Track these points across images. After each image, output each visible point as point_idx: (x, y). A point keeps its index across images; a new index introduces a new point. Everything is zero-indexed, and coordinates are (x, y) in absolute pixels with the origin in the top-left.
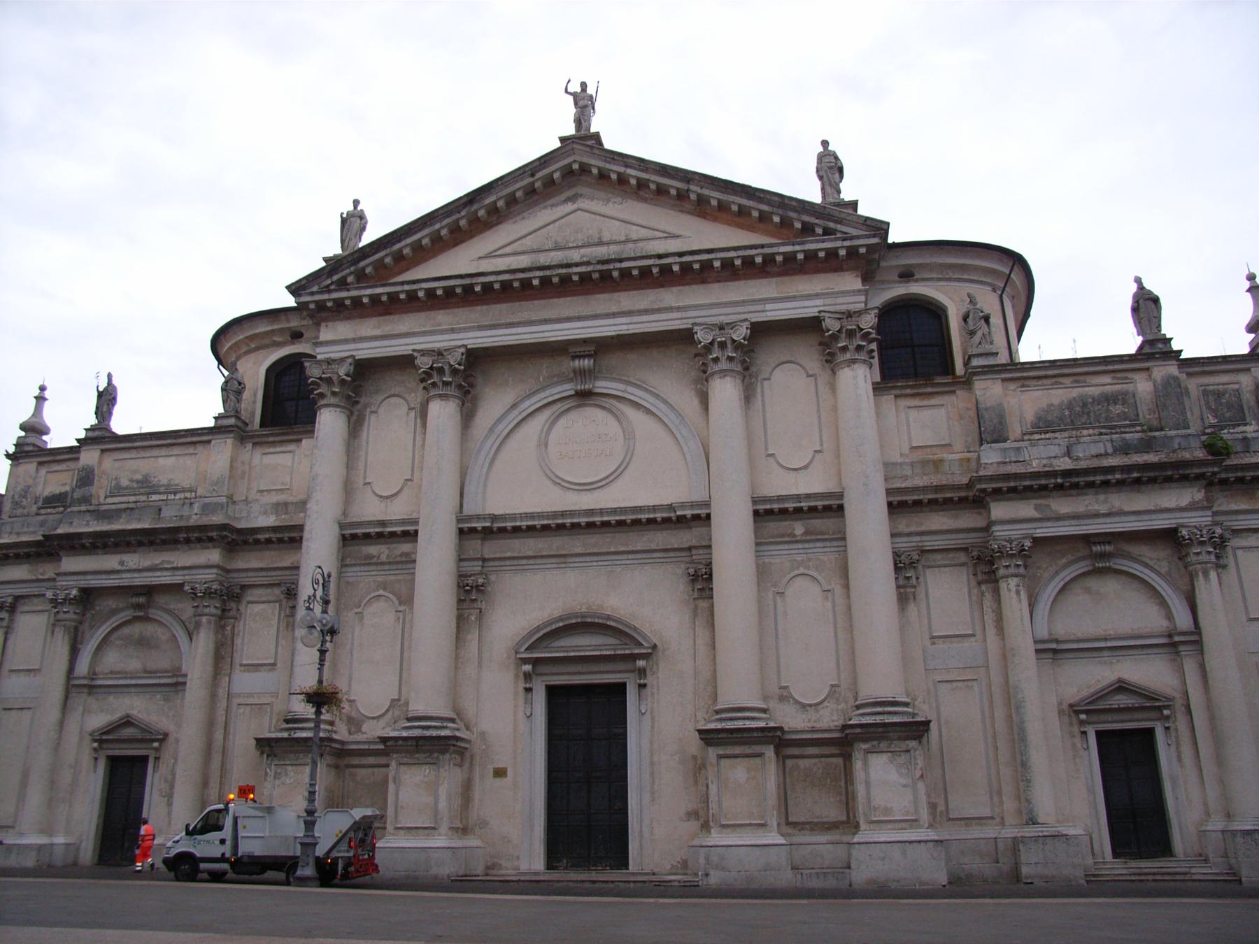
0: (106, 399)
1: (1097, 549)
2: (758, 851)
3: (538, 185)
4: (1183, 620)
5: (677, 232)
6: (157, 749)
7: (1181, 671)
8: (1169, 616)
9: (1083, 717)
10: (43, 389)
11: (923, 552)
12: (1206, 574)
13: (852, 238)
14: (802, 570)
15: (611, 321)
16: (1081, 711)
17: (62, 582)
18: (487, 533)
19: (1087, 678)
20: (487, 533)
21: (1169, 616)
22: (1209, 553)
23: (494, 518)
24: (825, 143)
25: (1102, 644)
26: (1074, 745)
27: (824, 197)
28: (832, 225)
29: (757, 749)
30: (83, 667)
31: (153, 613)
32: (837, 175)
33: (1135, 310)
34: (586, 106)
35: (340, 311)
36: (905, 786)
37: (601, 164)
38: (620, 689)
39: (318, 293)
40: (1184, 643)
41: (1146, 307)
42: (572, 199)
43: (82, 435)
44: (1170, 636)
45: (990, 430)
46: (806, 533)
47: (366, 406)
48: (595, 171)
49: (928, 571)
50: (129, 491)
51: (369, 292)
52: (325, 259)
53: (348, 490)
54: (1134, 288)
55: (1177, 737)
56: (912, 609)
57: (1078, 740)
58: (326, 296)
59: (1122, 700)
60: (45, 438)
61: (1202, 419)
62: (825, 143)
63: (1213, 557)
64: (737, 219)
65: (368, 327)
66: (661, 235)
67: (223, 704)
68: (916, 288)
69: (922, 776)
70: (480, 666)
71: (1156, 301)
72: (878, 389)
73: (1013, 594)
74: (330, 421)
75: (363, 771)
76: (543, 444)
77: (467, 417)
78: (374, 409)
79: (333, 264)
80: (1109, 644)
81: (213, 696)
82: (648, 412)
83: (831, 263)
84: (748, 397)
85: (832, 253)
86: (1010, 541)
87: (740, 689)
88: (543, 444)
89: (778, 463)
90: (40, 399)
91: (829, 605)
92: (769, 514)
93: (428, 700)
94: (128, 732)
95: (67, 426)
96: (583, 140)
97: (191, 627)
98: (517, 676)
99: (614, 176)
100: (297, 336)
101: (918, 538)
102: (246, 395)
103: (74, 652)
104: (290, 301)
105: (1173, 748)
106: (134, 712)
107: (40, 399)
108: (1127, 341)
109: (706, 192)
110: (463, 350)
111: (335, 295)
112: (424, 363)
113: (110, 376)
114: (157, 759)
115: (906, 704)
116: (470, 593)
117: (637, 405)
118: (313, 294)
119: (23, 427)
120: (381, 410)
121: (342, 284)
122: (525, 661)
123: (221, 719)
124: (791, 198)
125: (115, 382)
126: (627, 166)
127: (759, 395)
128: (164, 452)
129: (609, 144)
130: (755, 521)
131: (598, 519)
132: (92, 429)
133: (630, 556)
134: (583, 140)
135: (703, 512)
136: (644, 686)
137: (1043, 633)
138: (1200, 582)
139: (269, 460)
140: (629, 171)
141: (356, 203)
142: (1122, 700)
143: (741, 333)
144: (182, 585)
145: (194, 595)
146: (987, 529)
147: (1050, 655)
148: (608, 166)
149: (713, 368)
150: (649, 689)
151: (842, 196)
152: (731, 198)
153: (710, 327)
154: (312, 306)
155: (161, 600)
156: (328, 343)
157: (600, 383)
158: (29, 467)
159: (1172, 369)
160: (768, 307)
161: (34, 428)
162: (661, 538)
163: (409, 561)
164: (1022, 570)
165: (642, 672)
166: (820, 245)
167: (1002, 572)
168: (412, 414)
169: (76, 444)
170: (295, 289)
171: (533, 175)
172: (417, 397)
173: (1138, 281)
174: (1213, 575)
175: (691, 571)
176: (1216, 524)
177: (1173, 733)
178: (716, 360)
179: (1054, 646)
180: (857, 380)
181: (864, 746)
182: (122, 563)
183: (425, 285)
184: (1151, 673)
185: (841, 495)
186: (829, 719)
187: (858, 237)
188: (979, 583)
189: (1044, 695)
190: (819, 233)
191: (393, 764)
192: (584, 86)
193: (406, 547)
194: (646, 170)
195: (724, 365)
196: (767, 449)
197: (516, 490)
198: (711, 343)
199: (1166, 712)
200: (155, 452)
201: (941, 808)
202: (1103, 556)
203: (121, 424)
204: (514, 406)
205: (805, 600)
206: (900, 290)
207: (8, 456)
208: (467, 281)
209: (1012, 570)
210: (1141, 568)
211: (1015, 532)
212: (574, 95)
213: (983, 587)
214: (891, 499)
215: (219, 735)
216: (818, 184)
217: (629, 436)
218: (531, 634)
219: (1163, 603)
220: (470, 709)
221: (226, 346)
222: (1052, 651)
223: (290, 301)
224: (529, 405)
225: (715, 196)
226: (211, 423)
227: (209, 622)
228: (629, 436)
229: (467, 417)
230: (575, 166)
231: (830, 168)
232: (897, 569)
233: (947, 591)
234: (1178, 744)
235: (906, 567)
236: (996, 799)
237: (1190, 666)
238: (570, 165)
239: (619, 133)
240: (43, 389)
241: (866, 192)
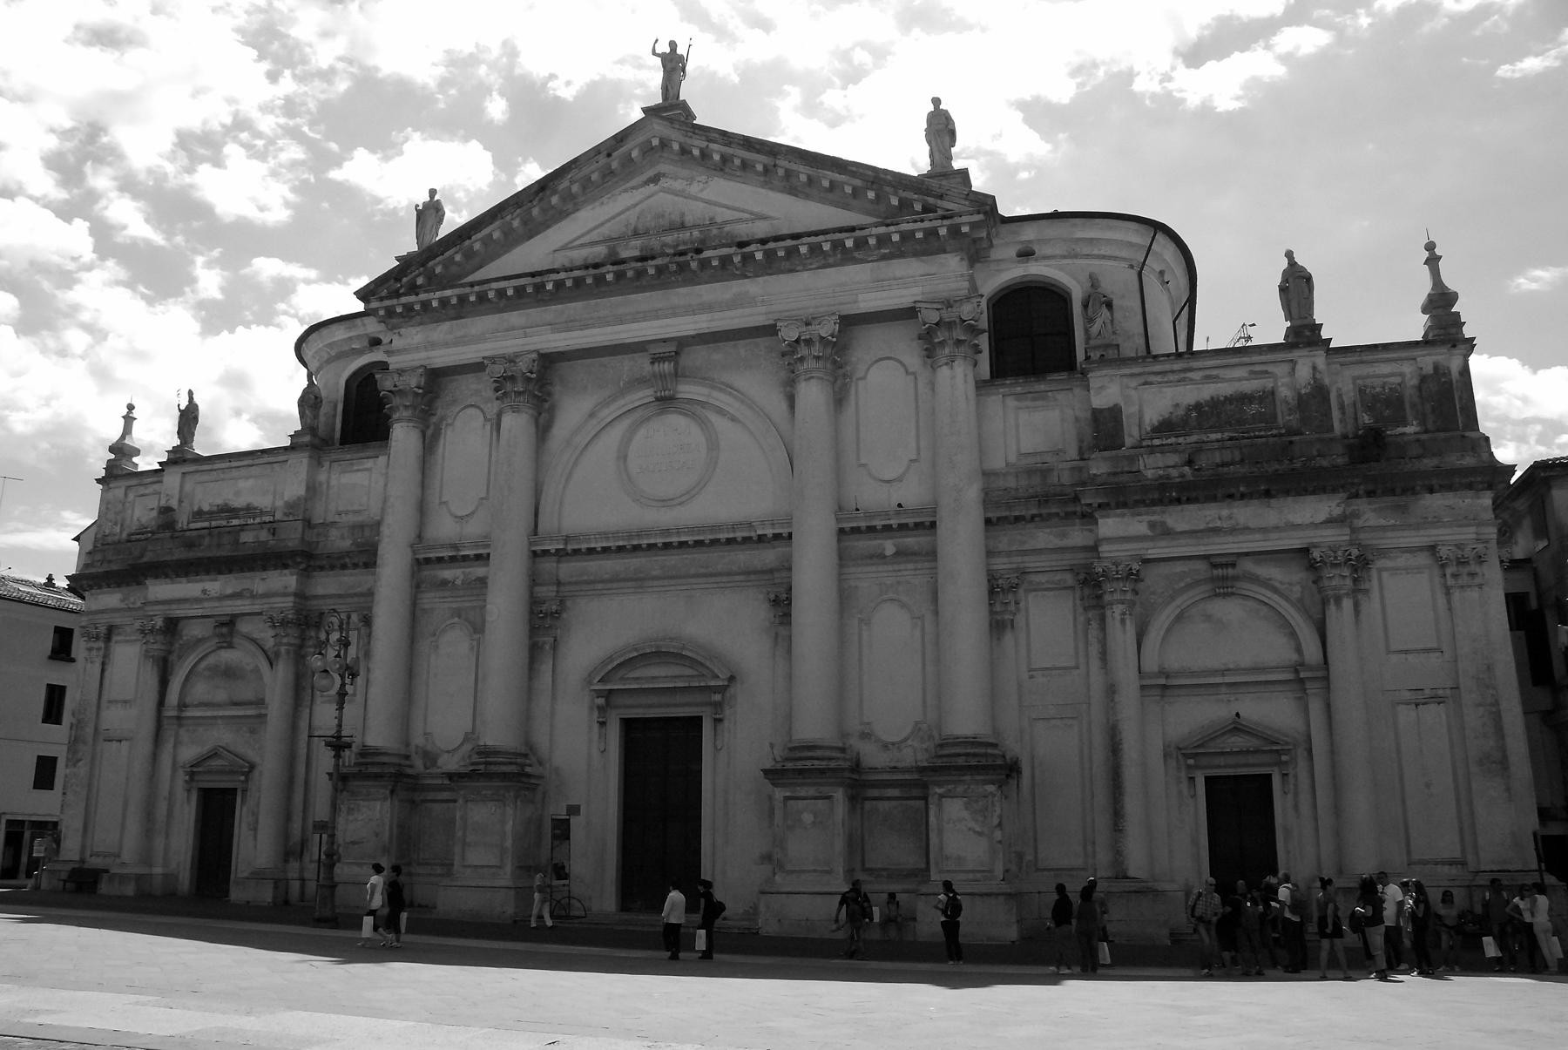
0: (188, 418)
2: (819, 899)
3: (615, 165)
4: (1312, 652)
7: (1306, 710)
9: (1191, 762)
10: (1430, 247)
11: (1146, 561)
12: (1338, 600)
14: (891, 595)
16: (1187, 754)
17: (151, 610)
18: (560, 554)
19: (1192, 716)
20: (560, 554)
22: (1344, 577)
23: (567, 539)
25: (1218, 680)
26: (1180, 792)
28: (931, 200)
29: (826, 790)
30: (173, 697)
32: (947, 139)
33: (1283, 290)
34: (674, 69)
36: (980, 834)
37: (682, 139)
38: (696, 722)
39: (386, 298)
40: (1310, 679)
42: (655, 179)
45: (1105, 429)
46: (897, 554)
47: (442, 419)
48: (676, 147)
49: (1031, 596)
50: (211, 515)
51: (438, 294)
52: (398, 259)
53: (422, 508)
54: (1285, 263)
55: (1296, 786)
56: (1008, 638)
57: (1184, 786)
58: (395, 301)
59: (1238, 742)
60: (135, 460)
61: (1356, 419)
63: (1349, 582)
64: (830, 196)
65: (442, 331)
67: (304, 736)
68: (1035, 269)
69: (1000, 825)
70: (554, 697)
71: (1308, 279)
72: (981, 386)
73: (1118, 624)
74: (403, 436)
75: (436, 806)
77: (543, 430)
78: (861, 374)
79: (406, 263)
80: (1228, 680)
81: (294, 728)
82: (733, 419)
83: (929, 246)
84: (839, 401)
85: (931, 233)
86: (1116, 564)
87: (813, 726)
89: (870, 474)
90: (1433, 261)
91: (918, 633)
92: (853, 532)
93: (499, 735)
94: (216, 763)
95: (155, 440)
96: (670, 110)
97: (272, 656)
98: (591, 708)
99: (696, 152)
100: (375, 342)
101: (1019, 559)
102: (325, 409)
103: (164, 682)
104: (359, 306)
105: (1290, 796)
107: (1433, 261)
109: (794, 167)
110: (534, 356)
111: (404, 300)
112: (790, 333)
113: (191, 393)
114: (245, 791)
116: (543, 622)
117: (721, 412)
118: (381, 299)
119: (111, 449)
120: (458, 423)
121: (413, 289)
122: (599, 693)
123: (302, 751)
124: (886, 171)
125: (196, 399)
126: (710, 141)
127: (852, 397)
128: (243, 472)
130: (987, 531)
131: (675, 539)
132: (175, 450)
133: (712, 580)
134: (670, 110)
135: (784, 531)
136: (720, 720)
137: (1150, 664)
138: (1332, 609)
139: (347, 479)
140: (713, 146)
142: (1238, 742)
143: (827, 329)
146: (1094, 548)
147: (1158, 692)
148: (689, 141)
149: (801, 368)
150: (726, 723)
158: (118, 491)
159: (1320, 359)
161: (122, 451)
162: (744, 558)
164: (1129, 596)
165: (718, 706)
167: (1107, 598)
168: (488, 427)
169: (158, 467)
170: (362, 294)
171: (609, 155)
172: (492, 408)
173: (1289, 255)
174: (1347, 604)
175: (772, 597)
176: (1351, 543)
177: (1291, 780)
178: (802, 359)
180: (958, 379)
181: (939, 791)
183: (495, 285)
184: (1274, 712)
185: (934, 512)
186: (911, 755)
188: (1085, 609)
191: (461, 801)
192: (673, 45)
193: (480, 571)
194: (728, 145)
195: (810, 364)
196: (858, 458)
198: (797, 341)
199: (1284, 758)
200: (235, 473)
201: (1029, 857)
204: (592, 415)
205: (891, 629)
206: (1014, 272)
207: (98, 481)
209: (1117, 596)
210: (1269, 594)
212: (663, 56)
213: (1090, 615)
214: (989, 515)
215: (301, 769)
217: (713, 445)
218: (604, 663)
219: (1293, 635)
220: (541, 739)
223: (359, 306)
224: (607, 414)
225: (803, 173)
226: (287, 442)
227: (288, 652)
228: (713, 445)
229: (543, 430)
230: (655, 142)
232: (992, 592)
233: (1049, 620)
234: (1296, 795)
235: (1002, 593)
236: (1090, 848)
237: (1316, 706)
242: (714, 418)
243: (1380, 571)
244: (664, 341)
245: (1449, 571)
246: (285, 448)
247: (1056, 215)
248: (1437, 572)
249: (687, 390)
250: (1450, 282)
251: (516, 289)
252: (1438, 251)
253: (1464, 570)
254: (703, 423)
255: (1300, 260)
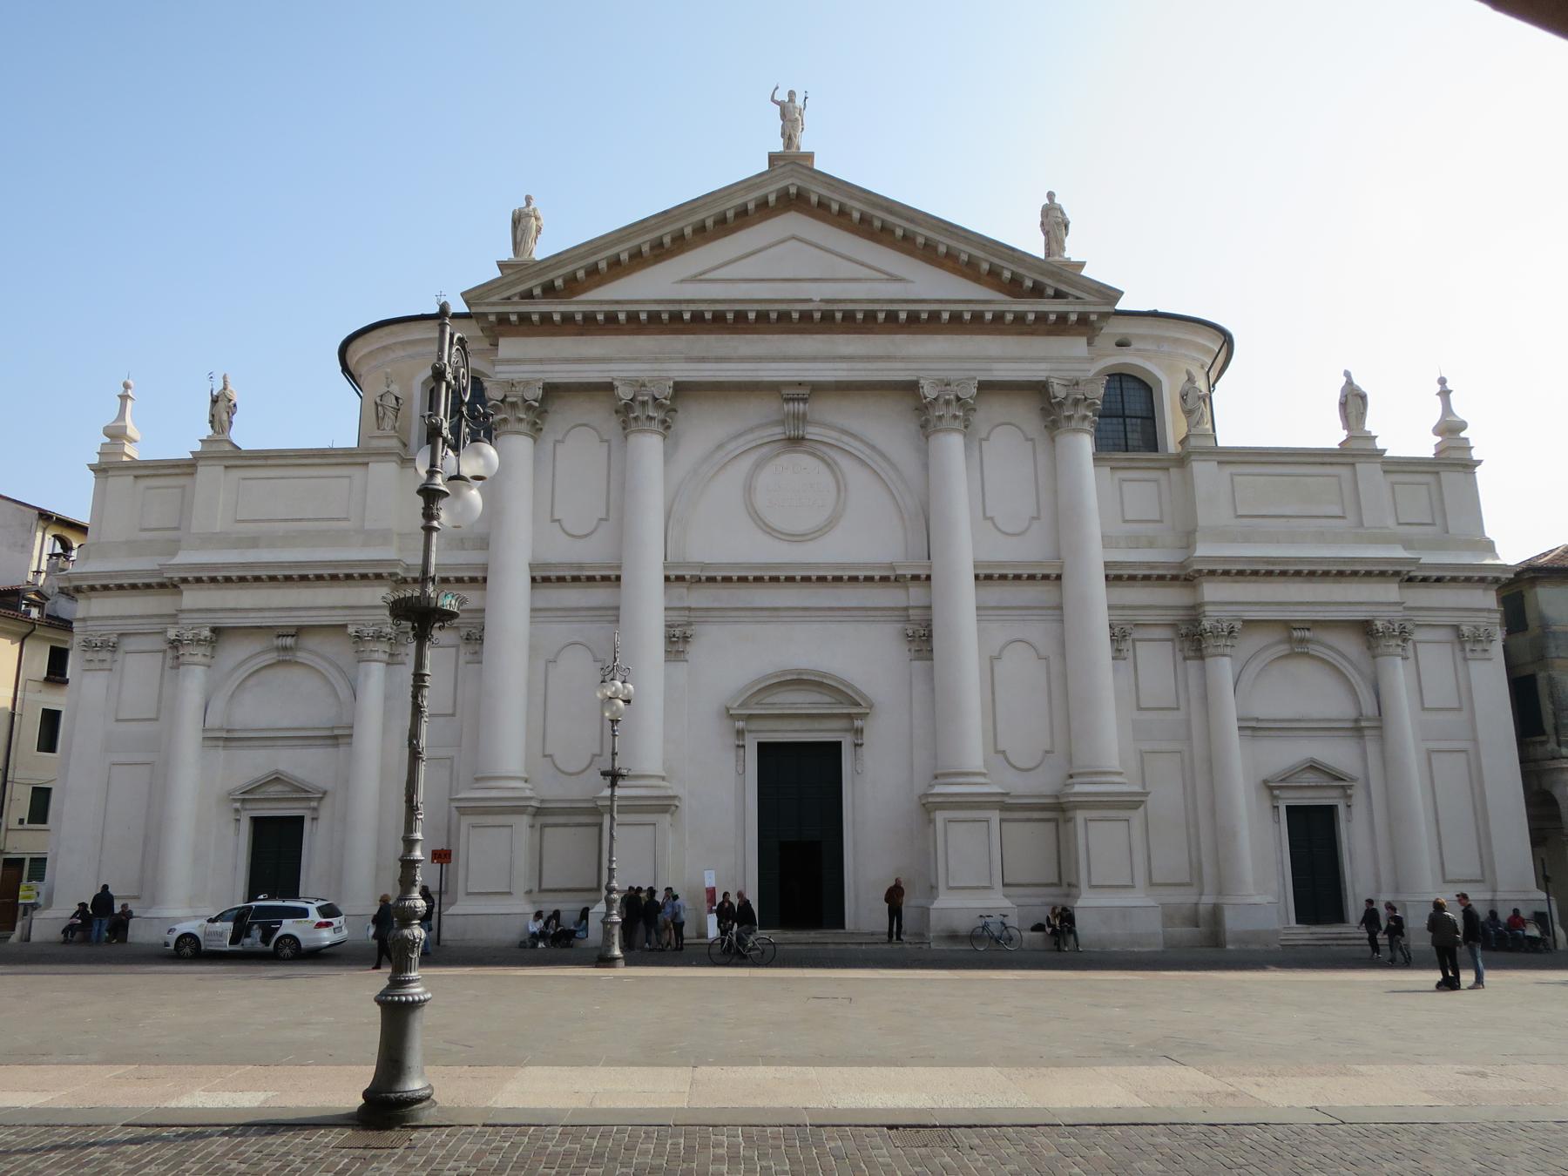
1: (1296, 634)
5: (904, 275)
6: (315, 809)
8: (1357, 702)
10: (1442, 381)
13: (1085, 303)
15: (830, 365)
16: (1271, 788)
19: (1286, 754)
21: (1357, 702)
24: (1051, 195)
27: (1048, 254)
28: (1064, 288)
31: (301, 656)
33: (1344, 405)
35: (525, 325)
40: (1369, 726)
41: (1353, 403)
43: (198, 447)
44: (1357, 720)
60: (1463, 435)
62: (1051, 195)
66: (879, 275)
71: (1363, 397)
76: (749, 489)
83: (1060, 326)
88: (749, 489)
90: (1445, 394)
96: (790, 160)
106: (282, 767)
107: (1445, 394)
108: (1331, 435)
112: (625, 393)
115: (1120, 774)
118: (494, 304)
129: (819, 165)
134: (790, 160)
137: (214, 720)
141: (528, 199)
142: (274, 790)
144: (345, 626)
145: (359, 637)
151: (1067, 255)
152: (962, 247)
153: (630, 382)
154: (492, 318)
155: (311, 642)
156: (509, 361)
157: (810, 429)
160: (995, 366)
163: (613, 614)
166: (1052, 307)
170: (467, 296)
173: (1347, 374)
179: (1254, 724)
182: (462, 602)
184: (1338, 754)
187: (1089, 303)
188: (1185, 659)
189: (1244, 769)
190: (1037, 294)
192: (792, 94)
197: (728, 542)
202: (1302, 641)
203: (246, 435)
204: (720, 446)
208: (676, 307)
211: (1226, 614)
216: (1042, 238)
217: (841, 486)
221: (357, 352)
222: (1252, 728)
228: (841, 486)
231: (1054, 222)
238: (787, 188)
239: (840, 156)
240: (1442, 381)
241: (1096, 254)
242: (845, 463)
243: (1134, 641)
244: (800, 384)
245: (1468, 647)
246: (347, 452)
247: (1154, 314)
248: (1457, 647)
249: (812, 432)
250: (1460, 410)
251: (650, 313)
252: (1449, 386)
253: (1478, 647)
254: (830, 465)
255: (1356, 381)
